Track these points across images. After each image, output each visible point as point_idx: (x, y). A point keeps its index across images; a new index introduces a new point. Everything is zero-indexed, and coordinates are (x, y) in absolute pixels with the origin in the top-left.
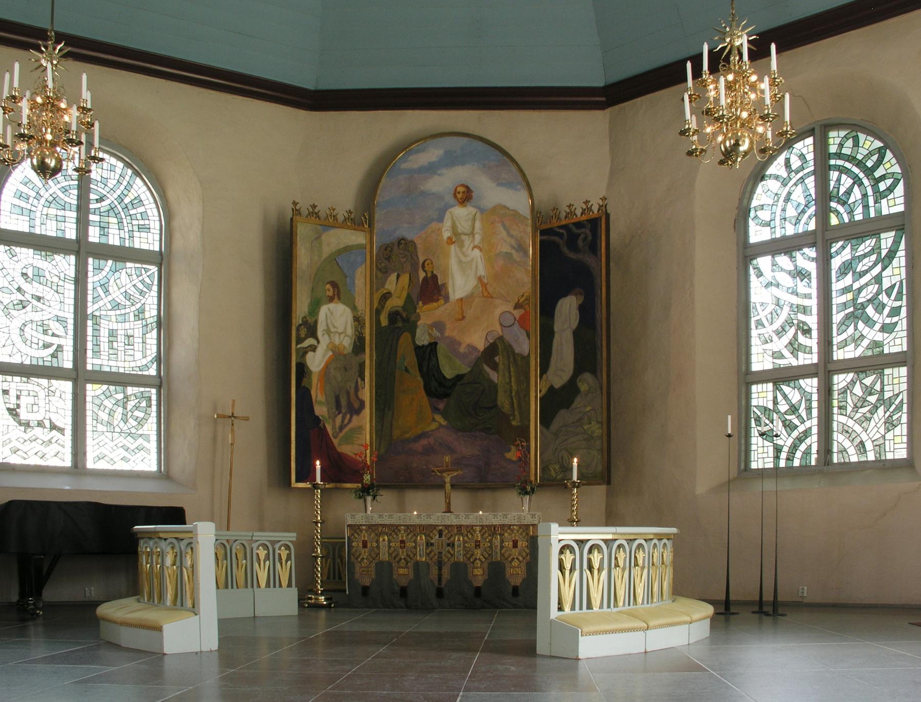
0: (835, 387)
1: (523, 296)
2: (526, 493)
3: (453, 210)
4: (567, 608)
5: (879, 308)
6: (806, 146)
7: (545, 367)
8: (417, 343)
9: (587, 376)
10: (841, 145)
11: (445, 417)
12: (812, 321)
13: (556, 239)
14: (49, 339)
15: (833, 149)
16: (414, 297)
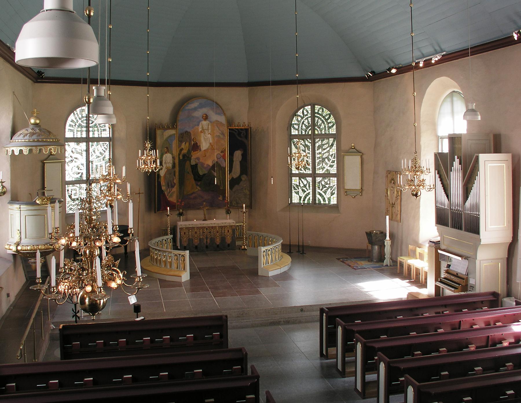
0: (317, 181)
1: (223, 149)
2: (229, 213)
5: (329, 160)
6: (308, 108)
7: (231, 171)
8: (191, 164)
10: (318, 111)
11: (200, 187)
12: (310, 161)
13: (234, 132)
14: (79, 171)
15: (316, 111)
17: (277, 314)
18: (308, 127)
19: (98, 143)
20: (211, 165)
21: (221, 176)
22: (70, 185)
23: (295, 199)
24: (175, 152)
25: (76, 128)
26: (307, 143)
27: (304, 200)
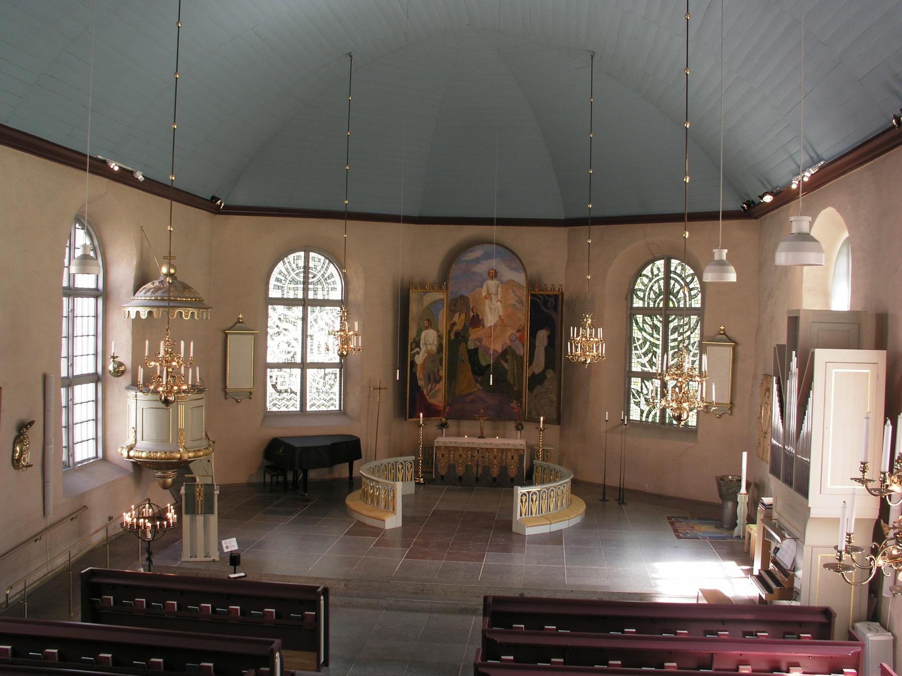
1: (521, 326)
2: (519, 430)
3: (488, 281)
4: (523, 516)
6: (660, 263)
7: (531, 362)
9: (551, 371)
10: (676, 268)
11: (481, 385)
13: (537, 299)
14: (290, 349)
15: (673, 269)
16: (468, 325)
17: (479, 596)
18: (660, 295)
19: (322, 308)
20: (500, 352)
21: (515, 370)
22: (275, 369)
23: (634, 413)
24: (443, 326)
25: (287, 284)
26: (656, 322)
27: (647, 417)
